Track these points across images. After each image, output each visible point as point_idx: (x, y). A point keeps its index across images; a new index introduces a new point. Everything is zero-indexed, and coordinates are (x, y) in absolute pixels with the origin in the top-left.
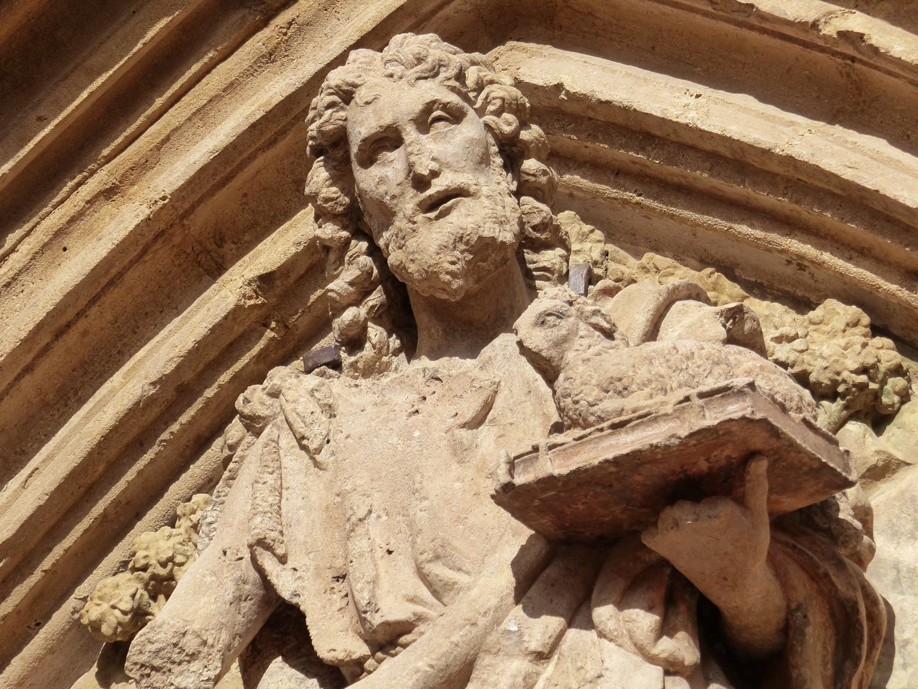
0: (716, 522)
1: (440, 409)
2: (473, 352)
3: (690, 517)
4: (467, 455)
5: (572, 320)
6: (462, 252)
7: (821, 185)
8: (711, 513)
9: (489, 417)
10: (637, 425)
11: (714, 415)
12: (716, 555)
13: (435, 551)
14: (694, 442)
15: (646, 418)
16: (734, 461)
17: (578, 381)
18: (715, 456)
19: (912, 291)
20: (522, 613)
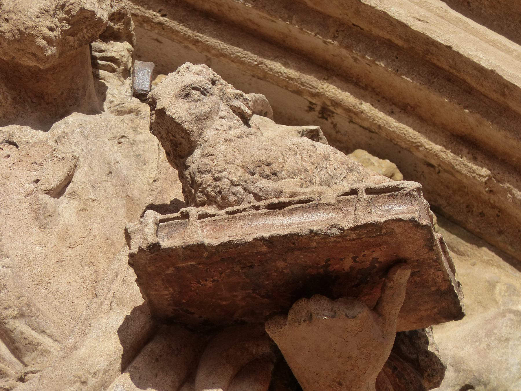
0: (351, 323)
1: (17, 172)
2: (45, 125)
3: (327, 313)
4: (51, 221)
5: (214, 98)
6: (60, 20)
7: (381, 33)
8: (350, 313)
9: (69, 189)
10: (296, 209)
11: (380, 213)
12: (339, 357)
13: (20, 309)
14: (354, 236)
15: (307, 204)
16: (377, 265)
17: (221, 159)
18: (364, 256)
19: (458, 155)
20: (129, 381)
